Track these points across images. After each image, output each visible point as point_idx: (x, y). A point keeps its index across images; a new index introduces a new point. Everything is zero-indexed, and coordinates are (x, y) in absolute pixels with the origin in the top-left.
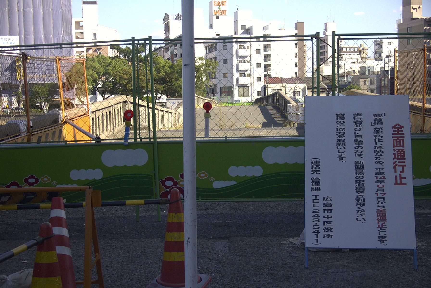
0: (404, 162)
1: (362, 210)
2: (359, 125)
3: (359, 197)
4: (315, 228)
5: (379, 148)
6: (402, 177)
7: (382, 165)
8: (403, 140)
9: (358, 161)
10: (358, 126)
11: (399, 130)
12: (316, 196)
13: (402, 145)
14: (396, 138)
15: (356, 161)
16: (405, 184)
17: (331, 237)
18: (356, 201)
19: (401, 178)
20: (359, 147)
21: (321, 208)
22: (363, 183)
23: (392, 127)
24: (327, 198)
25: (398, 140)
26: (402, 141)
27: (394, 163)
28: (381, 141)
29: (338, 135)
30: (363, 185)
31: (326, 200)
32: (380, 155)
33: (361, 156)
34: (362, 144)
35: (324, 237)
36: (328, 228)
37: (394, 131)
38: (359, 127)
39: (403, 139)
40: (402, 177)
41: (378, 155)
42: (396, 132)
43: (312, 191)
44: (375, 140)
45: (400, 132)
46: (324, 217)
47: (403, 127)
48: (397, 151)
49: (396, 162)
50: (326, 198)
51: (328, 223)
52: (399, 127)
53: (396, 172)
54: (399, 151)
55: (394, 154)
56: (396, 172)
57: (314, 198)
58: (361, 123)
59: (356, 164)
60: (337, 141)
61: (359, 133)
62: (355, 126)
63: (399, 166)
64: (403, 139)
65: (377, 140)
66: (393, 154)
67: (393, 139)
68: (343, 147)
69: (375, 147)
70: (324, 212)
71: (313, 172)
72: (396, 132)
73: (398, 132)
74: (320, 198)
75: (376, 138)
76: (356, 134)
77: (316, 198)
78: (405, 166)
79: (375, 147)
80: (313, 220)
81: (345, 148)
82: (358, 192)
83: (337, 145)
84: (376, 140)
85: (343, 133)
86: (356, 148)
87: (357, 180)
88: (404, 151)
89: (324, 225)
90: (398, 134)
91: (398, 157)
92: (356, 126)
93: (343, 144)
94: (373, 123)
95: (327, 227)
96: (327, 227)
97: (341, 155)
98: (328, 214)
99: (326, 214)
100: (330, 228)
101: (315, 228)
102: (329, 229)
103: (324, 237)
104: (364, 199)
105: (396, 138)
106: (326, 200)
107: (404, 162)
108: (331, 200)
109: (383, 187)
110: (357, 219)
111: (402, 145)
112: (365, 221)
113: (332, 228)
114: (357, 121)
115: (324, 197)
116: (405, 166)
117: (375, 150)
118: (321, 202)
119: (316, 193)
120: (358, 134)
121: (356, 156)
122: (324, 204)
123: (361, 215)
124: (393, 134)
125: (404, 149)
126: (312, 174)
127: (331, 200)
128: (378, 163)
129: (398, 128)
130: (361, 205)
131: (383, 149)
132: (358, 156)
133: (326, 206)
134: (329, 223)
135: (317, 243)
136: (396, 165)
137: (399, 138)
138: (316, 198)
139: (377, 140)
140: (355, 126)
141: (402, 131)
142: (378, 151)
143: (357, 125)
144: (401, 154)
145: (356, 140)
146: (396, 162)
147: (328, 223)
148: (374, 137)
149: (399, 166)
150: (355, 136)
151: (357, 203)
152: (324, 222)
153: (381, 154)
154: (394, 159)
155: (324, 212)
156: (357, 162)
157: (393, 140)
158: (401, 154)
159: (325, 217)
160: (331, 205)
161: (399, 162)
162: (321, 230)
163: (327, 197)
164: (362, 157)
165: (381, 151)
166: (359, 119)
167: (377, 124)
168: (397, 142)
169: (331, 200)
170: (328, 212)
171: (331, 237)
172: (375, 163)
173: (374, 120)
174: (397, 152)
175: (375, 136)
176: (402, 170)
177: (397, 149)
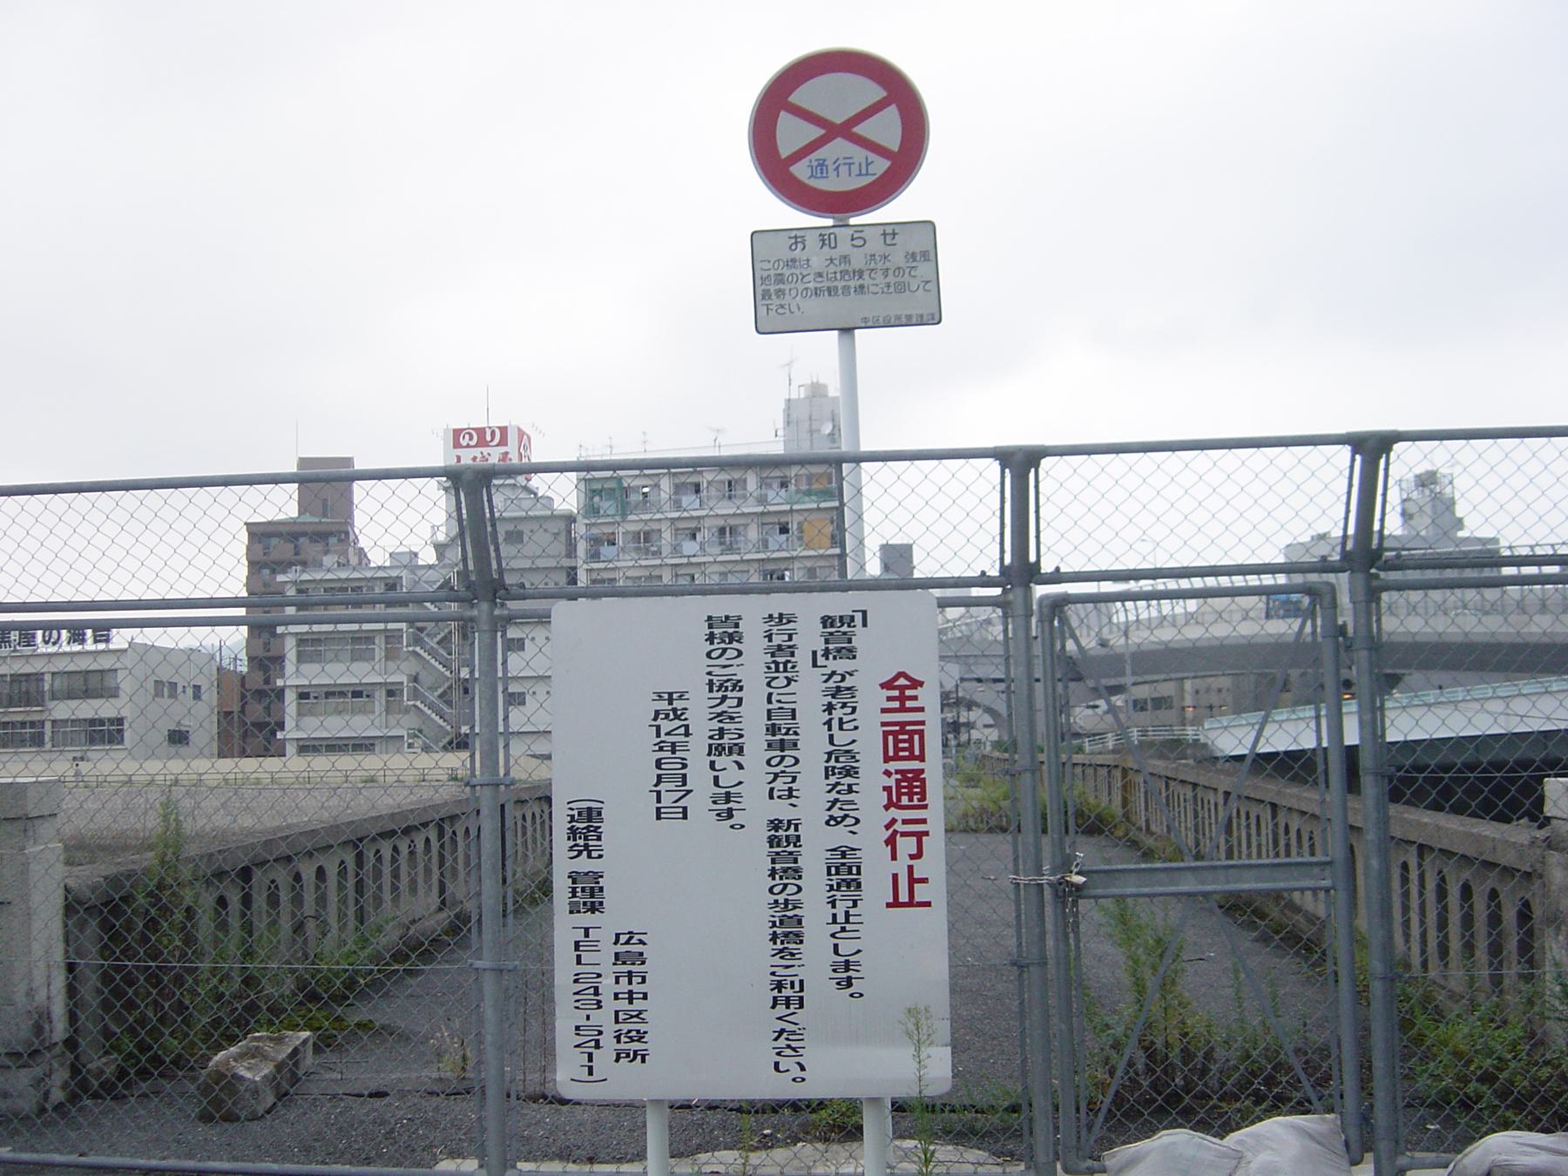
0: (924, 821)
1: (792, 1027)
2: (785, 664)
3: (780, 971)
4: (582, 1033)
5: (841, 759)
6: (916, 876)
7: (851, 832)
8: (921, 733)
9: (781, 822)
10: (781, 666)
11: (908, 693)
12: (587, 930)
13: (917, 752)
14: (897, 728)
15: (772, 822)
16: (928, 904)
17: (643, 1061)
18: (772, 990)
19: (912, 881)
20: (783, 758)
21: (608, 969)
22: (797, 912)
23: (883, 686)
24: (631, 938)
25: (903, 734)
26: (916, 737)
27: (887, 827)
28: (850, 726)
29: (719, 710)
30: (800, 922)
31: (627, 943)
32: (846, 787)
33: (790, 796)
34: (795, 745)
35: (617, 1060)
36: (629, 1031)
37: (889, 699)
38: (785, 670)
39: (923, 731)
40: (916, 876)
41: (839, 788)
42: (896, 704)
43: (571, 912)
44: (829, 723)
45: (909, 704)
46: (616, 996)
47: (921, 684)
48: (899, 776)
49: (894, 821)
50: (623, 939)
51: (632, 1017)
52: (908, 683)
53: (894, 857)
54: (905, 779)
55: (887, 789)
56: (894, 857)
57: (580, 935)
58: (792, 654)
59: (773, 832)
60: (711, 737)
61: (783, 698)
62: (769, 668)
63: (904, 834)
64: (923, 731)
65: (835, 724)
66: (885, 788)
67: (884, 732)
68: (736, 762)
69: (830, 754)
70: (617, 982)
71: (576, 853)
72: (896, 704)
73: (902, 704)
74: (604, 937)
75: (830, 714)
76: (773, 700)
77: (587, 935)
78: (926, 833)
79: (830, 754)
80: (577, 1004)
81: (741, 767)
82: (781, 951)
83: (709, 754)
84: (833, 721)
85: (736, 700)
86: (773, 762)
87: (776, 902)
88: (922, 776)
89: (617, 1021)
90: (902, 709)
91: (899, 799)
92: (773, 666)
93: (736, 749)
94: (820, 653)
95: (625, 1027)
96: (625, 1027)
97: (728, 797)
98: (630, 987)
99: (624, 986)
100: (638, 1032)
101: (582, 1033)
102: (634, 1033)
103: (617, 1060)
104: (801, 982)
105: (897, 728)
106: (627, 943)
107: (924, 821)
108: (641, 942)
109: (685, 766)
110: (777, 1065)
111: (917, 752)
112: (802, 1074)
113: (645, 1033)
114: (779, 646)
115: (618, 936)
116: (926, 833)
117: (826, 768)
118: (608, 950)
119: (587, 919)
120: (779, 701)
121: (771, 797)
122: (617, 954)
123: (789, 1046)
124: (884, 711)
125: (922, 771)
126: (571, 858)
127: (645, 944)
128: (838, 823)
129: (901, 688)
130: (788, 1007)
131: (857, 761)
132: (779, 797)
133: (624, 963)
134: (637, 1016)
135: (591, 1078)
136: (895, 832)
137: (908, 728)
138: (587, 935)
139: (835, 724)
140: (769, 668)
141: (915, 698)
142: (840, 773)
143: (777, 664)
144: (910, 787)
145: (773, 729)
146: (894, 821)
147: (632, 1017)
148: (824, 711)
149: (904, 834)
150: (769, 711)
151: (775, 999)
152: (617, 1013)
153: (850, 786)
154: (887, 808)
155: (617, 982)
156: (775, 825)
157: (886, 734)
158: (910, 787)
159: (620, 996)
160: (641, 958)
161: (905, 822)
162: (608, 1040)
163: (629, 933)
164: (793, 801)
165: (848, 774)
166: (786, 637)
167: (835, 658)
168: (896, 741)
169: (645, 944)
170: (630, 983)
171: (643, 1061)
172: (827, 823)
173: (823, 639)
174: (897, 780)
175: (830, 708)
176: (914, 851)
177: (897, 772)
